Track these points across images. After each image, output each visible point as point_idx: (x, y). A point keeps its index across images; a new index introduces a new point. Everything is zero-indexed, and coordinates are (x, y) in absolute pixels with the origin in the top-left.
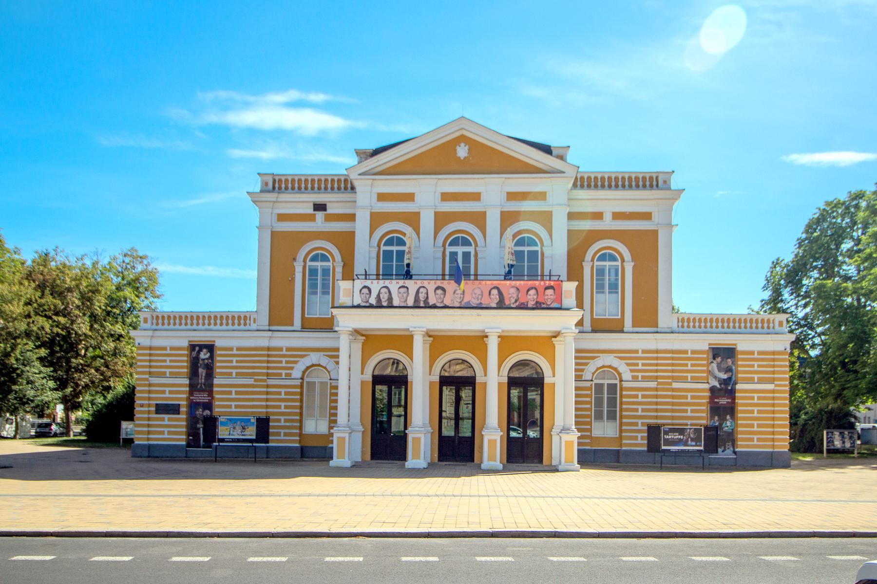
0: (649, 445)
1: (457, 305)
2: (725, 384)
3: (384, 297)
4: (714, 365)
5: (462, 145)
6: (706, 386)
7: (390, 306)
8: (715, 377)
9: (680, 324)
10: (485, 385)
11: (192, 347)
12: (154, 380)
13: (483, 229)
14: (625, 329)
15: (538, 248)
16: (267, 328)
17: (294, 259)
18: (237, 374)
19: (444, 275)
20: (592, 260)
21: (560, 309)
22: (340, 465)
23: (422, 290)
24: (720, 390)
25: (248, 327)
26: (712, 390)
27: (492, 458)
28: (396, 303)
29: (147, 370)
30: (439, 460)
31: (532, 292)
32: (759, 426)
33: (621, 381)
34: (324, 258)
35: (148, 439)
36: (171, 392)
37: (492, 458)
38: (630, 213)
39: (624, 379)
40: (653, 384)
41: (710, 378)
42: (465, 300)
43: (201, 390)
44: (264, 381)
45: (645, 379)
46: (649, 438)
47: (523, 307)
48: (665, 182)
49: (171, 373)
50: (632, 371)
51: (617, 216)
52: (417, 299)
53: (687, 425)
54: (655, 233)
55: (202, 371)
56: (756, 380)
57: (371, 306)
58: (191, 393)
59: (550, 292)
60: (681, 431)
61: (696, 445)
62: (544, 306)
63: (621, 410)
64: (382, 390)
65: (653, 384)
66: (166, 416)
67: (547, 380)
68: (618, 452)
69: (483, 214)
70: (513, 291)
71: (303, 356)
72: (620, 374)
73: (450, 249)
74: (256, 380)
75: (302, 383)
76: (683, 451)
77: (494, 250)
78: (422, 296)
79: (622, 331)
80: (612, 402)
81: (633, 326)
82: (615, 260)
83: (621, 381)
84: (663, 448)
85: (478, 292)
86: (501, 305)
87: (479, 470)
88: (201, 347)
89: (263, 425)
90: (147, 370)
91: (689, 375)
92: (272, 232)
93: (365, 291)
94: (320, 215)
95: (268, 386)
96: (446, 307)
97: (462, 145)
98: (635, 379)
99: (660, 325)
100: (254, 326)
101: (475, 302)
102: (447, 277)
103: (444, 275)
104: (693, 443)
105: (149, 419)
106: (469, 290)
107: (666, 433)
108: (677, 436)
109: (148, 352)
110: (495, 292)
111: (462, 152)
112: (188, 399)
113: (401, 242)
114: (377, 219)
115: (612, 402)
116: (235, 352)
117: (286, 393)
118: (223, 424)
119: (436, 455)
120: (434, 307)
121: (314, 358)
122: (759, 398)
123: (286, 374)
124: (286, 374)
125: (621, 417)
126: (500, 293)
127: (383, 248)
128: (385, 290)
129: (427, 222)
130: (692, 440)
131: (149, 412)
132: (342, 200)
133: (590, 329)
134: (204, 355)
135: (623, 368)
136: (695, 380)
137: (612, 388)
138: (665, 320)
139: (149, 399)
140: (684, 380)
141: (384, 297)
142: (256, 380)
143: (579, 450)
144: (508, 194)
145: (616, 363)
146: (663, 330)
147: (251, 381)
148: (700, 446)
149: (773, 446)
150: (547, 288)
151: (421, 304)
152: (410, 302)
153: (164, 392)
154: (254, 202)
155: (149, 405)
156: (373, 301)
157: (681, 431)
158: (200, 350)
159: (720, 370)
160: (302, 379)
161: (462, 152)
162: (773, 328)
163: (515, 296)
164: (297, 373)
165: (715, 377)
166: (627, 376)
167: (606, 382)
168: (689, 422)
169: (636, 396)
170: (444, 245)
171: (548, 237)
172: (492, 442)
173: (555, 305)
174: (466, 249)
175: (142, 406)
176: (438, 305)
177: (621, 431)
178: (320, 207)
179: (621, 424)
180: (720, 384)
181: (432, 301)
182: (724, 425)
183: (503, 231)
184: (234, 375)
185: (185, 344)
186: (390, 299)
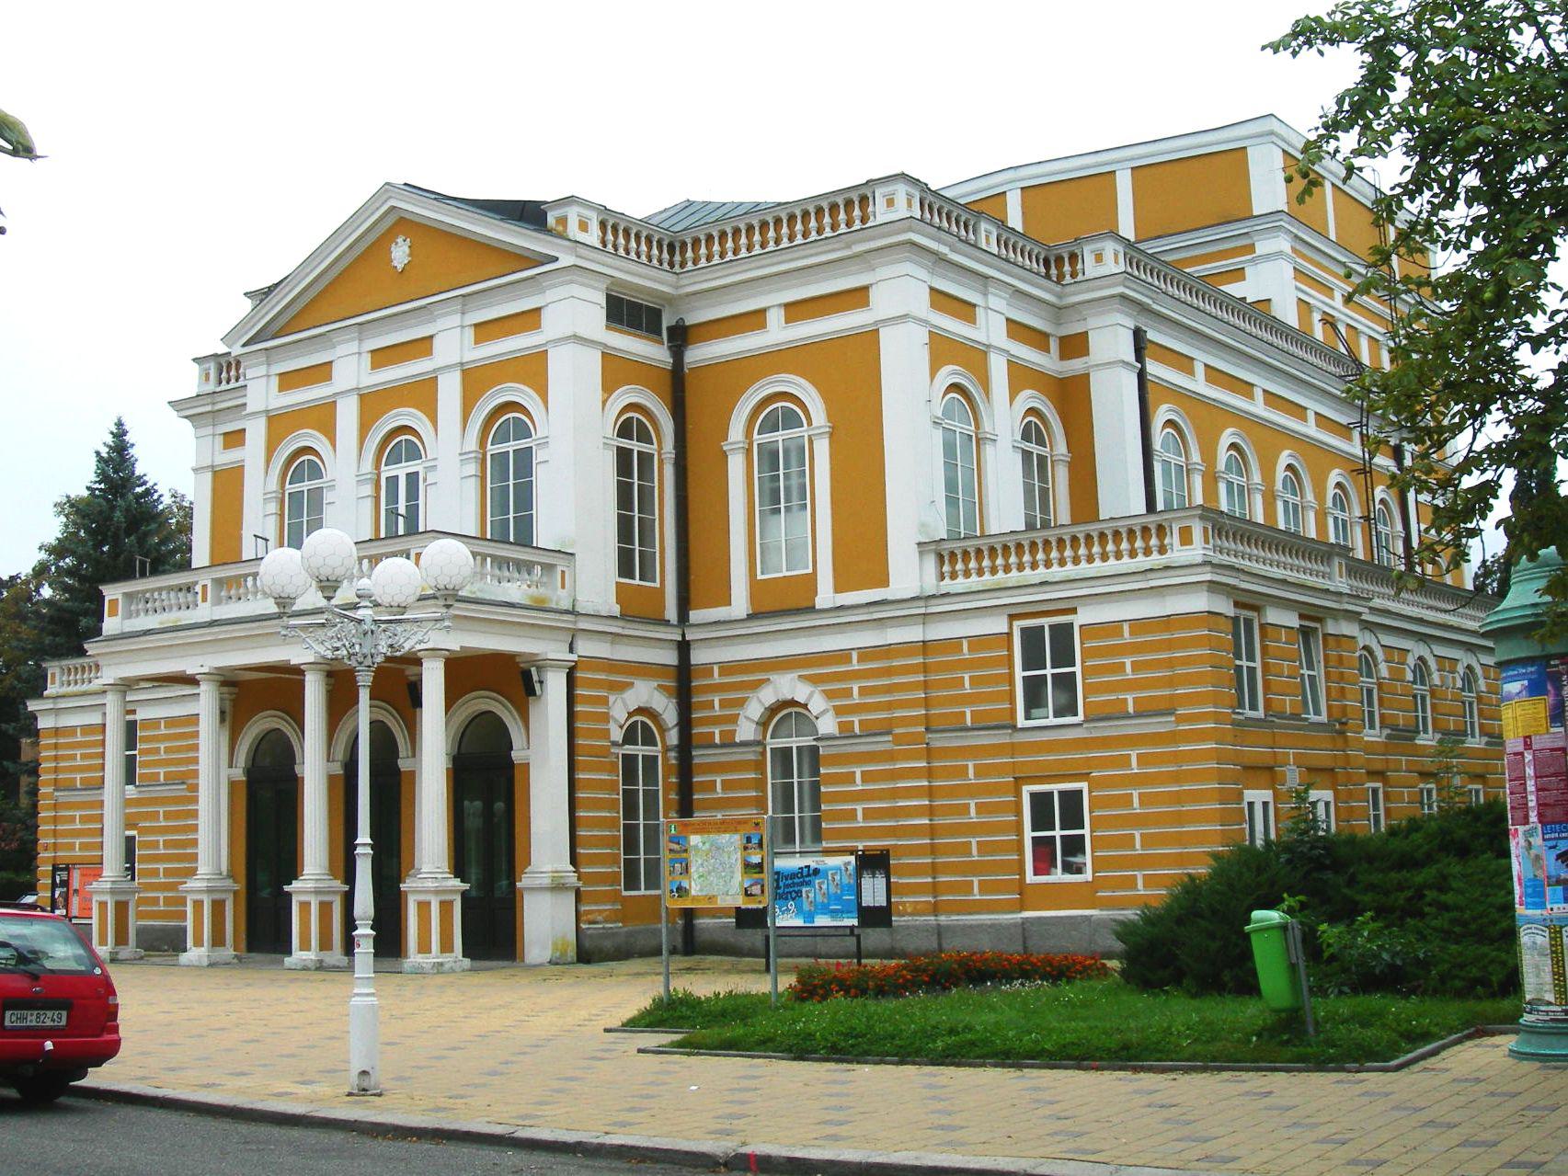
5: (400, 240)
34: (791, 420)
45: (871, 731)
50: (839, 711)
51: (796, 311)
65: (883, 743)
73: (387, 472)
79: (811, 609)
121: (787, 686)
129: (450, 391)
142: (898, 740)
145: (801, 692)
160: (761, 743)
166: (827, 725)
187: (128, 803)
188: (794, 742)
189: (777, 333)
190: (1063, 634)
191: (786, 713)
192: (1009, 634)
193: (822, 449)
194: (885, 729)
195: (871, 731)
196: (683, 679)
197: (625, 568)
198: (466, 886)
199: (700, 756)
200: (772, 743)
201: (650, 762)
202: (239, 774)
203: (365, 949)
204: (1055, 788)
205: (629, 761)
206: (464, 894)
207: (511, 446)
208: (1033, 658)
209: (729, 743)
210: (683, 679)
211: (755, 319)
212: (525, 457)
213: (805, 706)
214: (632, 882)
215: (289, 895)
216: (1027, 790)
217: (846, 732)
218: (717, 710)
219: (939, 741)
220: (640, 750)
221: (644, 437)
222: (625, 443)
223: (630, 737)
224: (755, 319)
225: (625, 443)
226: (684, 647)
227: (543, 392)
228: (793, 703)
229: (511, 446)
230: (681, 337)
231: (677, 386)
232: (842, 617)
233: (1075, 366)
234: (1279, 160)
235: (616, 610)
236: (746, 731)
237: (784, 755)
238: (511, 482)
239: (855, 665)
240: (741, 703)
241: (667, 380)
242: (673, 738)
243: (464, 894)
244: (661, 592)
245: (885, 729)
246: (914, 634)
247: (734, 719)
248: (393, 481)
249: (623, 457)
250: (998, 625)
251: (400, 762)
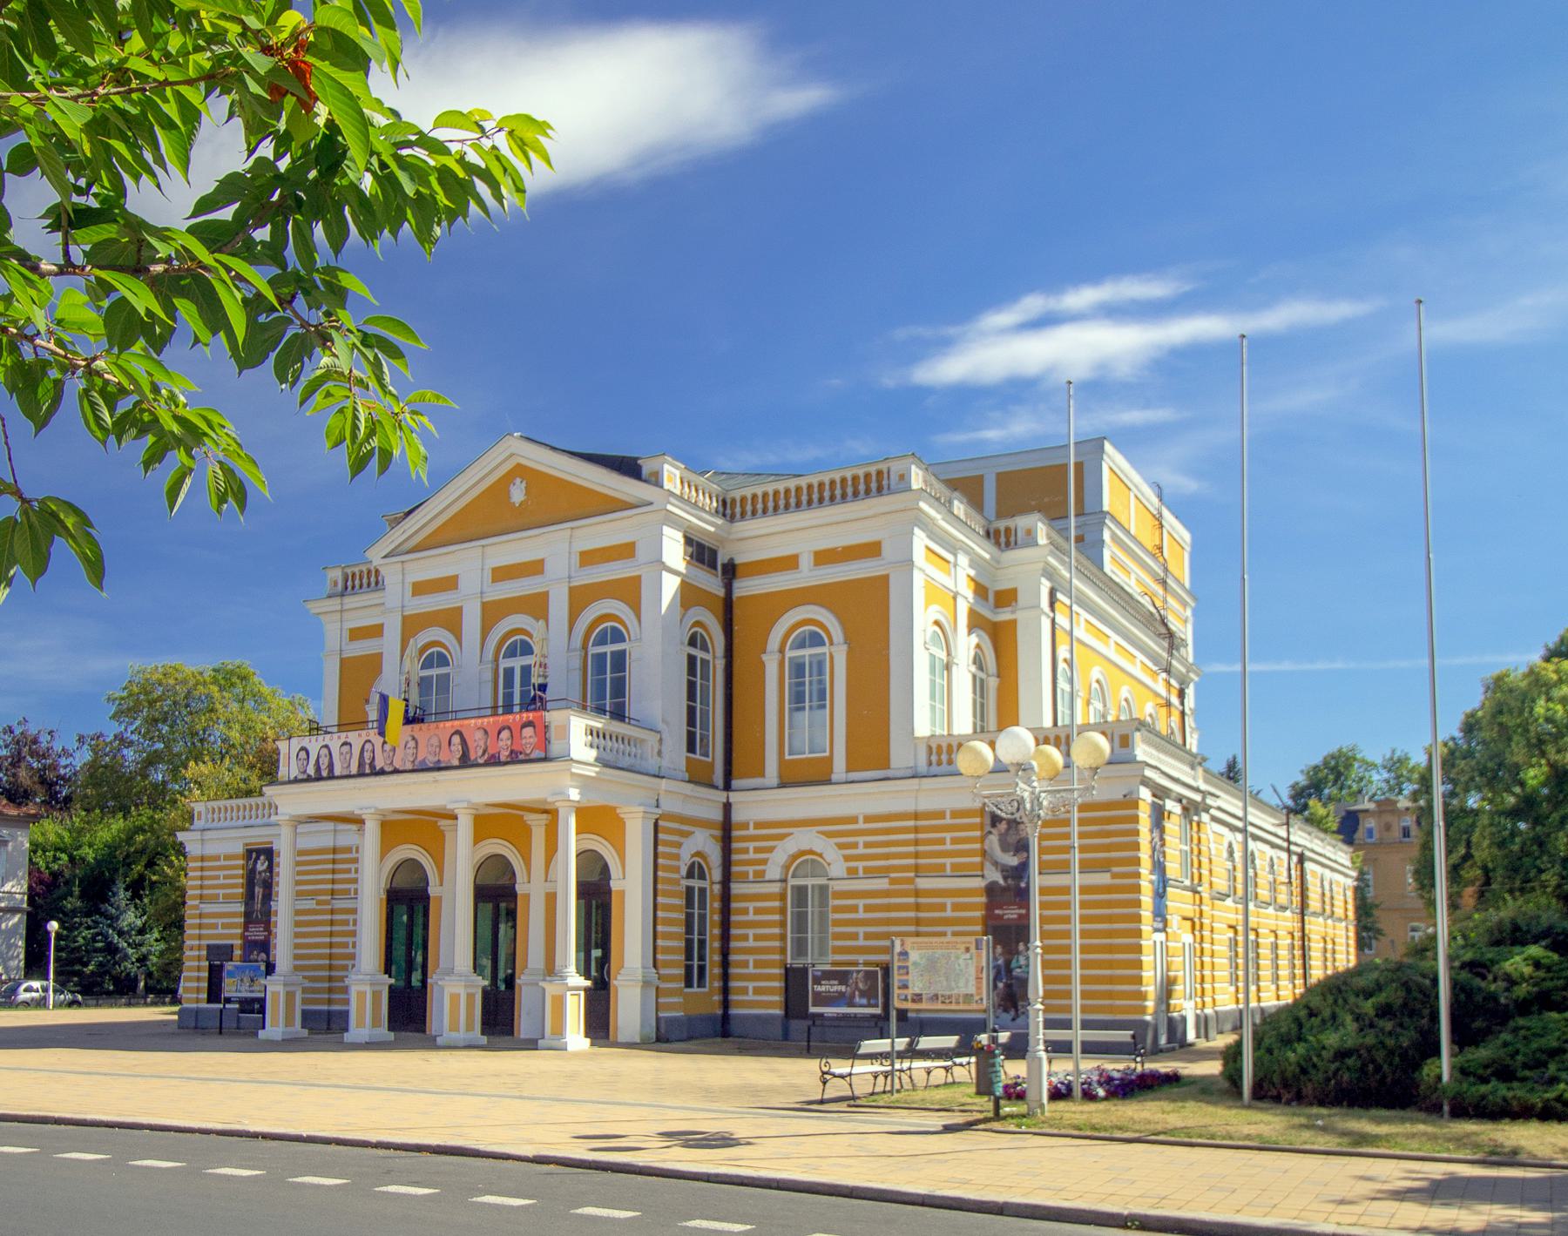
1: (409, 766)
2: (1013, 878)
3: (324, 762)
4: (994, 839)
5: (518, 480)
6: (979, 883)
7: (331, 777)
8: (996, 864)
9: (934, 758)
10: (622, 893)
11: (249, 852)
13: (457, 632)
14: (834, 777)
17: (367, 701)
18: (954, 867)
19: (495, 707)
20: (782, 651)
21: (545, 759)
23: (368, 746)
24: (1005, 890)
26: (991, 890)
27: (454, 1027)
28: (337, 771)
29: (912, 861)
31: (505, 734)
34: (816, 640)
37: (454, 1027)
38: (846, 549)
40: (882, 884)
41: (988, 865)
42: (420, 758)
43: (257, 922)
44: (910, 881)
45: (871, 873)
47: (494, 761)
48: (902, 477)
49: (225, 896)
50: (847, 858)
51: (824, 558)
52: (361, 764)
53: (856, 964)
54: (885, 579)
55: (258, 891)
56: (751, 877)
57: (309, 779)
58: (246, 927)
59: (528, 731)
60: (842, 977)
61: (869, 1005)
62: (521, 757)
65: (882, 884)
67: (433, 890)
69: (459, 611)
70: (479, 735)
71: (781, 837)
73: (505, 664)
74: (893, 881)
76: (845, 1017)
77: (472, 667)
78: (367, 755)
79: (828, 782)
81: (848, 770)
84: (813, 1010)
85: (435, 741)
86: (466, 762)
87: (432, 1044)
88: (259, 852)
90: (912, 861)
91: (948, 861)
92: (342, 660)
93: (303, 754)
95: (332, 912)
96: (396, 771)
97: (518, 480)
98: (852, 873)
99: (894, 764)
101: (431, 760)
102: (500, 711)
103: (495, 707)
104: (864, 1001)
106: (431, 737)
107: (817, 981)
108: (834, 987)
109: (911, 823)
110: (456, 739)
111: (518, 494)
112: (243, 937)
113: (618, 636)
114: (412, 625)
116: (861, 825)
117: (868, 908)
118: (231, 974)
120: (382, 772)
122: (956, 907)
123: (756, 873)
124: (756, 873)
126: (464, 742)
127: (593, 650)
128: (325, 751)
129: (559, 607)
130: (862, 994)
132: (814, 523)
133: (775, 781)
134: (261, 866)
136: (960, 872)
140: (939, 871)
141: (324, 762)
142: (893, 881)
144: (583, 554)
146: (899, 774)
148: (876, 1006)
150: (525, 726)
151: (366, 770)
152: (354, 770)
156: (311, 771)
157: (842, 977)
158: (258, 858)
159: (1005, 847)
160: (784, 881)
161: (518, 494)
163: (482, 743)
165: (996, 864)
166: (838, 868)
168: (861, 959)
169: (942, 907)
171: (636, 622)
172: (455, 998)
173: (537, 754)
176: (388, 769)
180: (1005, 878)
181: (379, 765)
182: (1014, 964)
183: (485, 631)
184: (861, 874)
185: (240, 850)
186: (331, 766)
187: (298, 912)
188: (809, 882)
189: (807, 576)
191: (807, 861)
196: (726, 831)
197: (691, 747)
198: (392, 981)
199: (736, 888)
200: (792, 882)
201: (702, 891)
205: (690, 890)
206: (391, 987)
207: (609, 649)
210: (726, 831)
212: (620, 660)
213: (821, 855)
214: (689, 984)
218: (751, 855)
219: (924, 883)
220: (696, 883)
221: (705, 648)
222: (694, 652)
223: (690, 875)
225: (694, 652)
226: (727, 807)
227: (636, 608)
228: (811, 852)
229: (609, 649)
230: (730, 572)
231: (727, 610)
233: (1004, 616)
234: (679, 536)
235: (687, 776)
236: (773, 872)
237: (801, 892)
238: (608, 676)
240: (771, 850)
241: (720, 607)
242: (717, 875)
243: (391, 987)
244: (712, 765)
247: (764, 862)
248: (509, 673)
249: (692, 660)
251: (612, 883)
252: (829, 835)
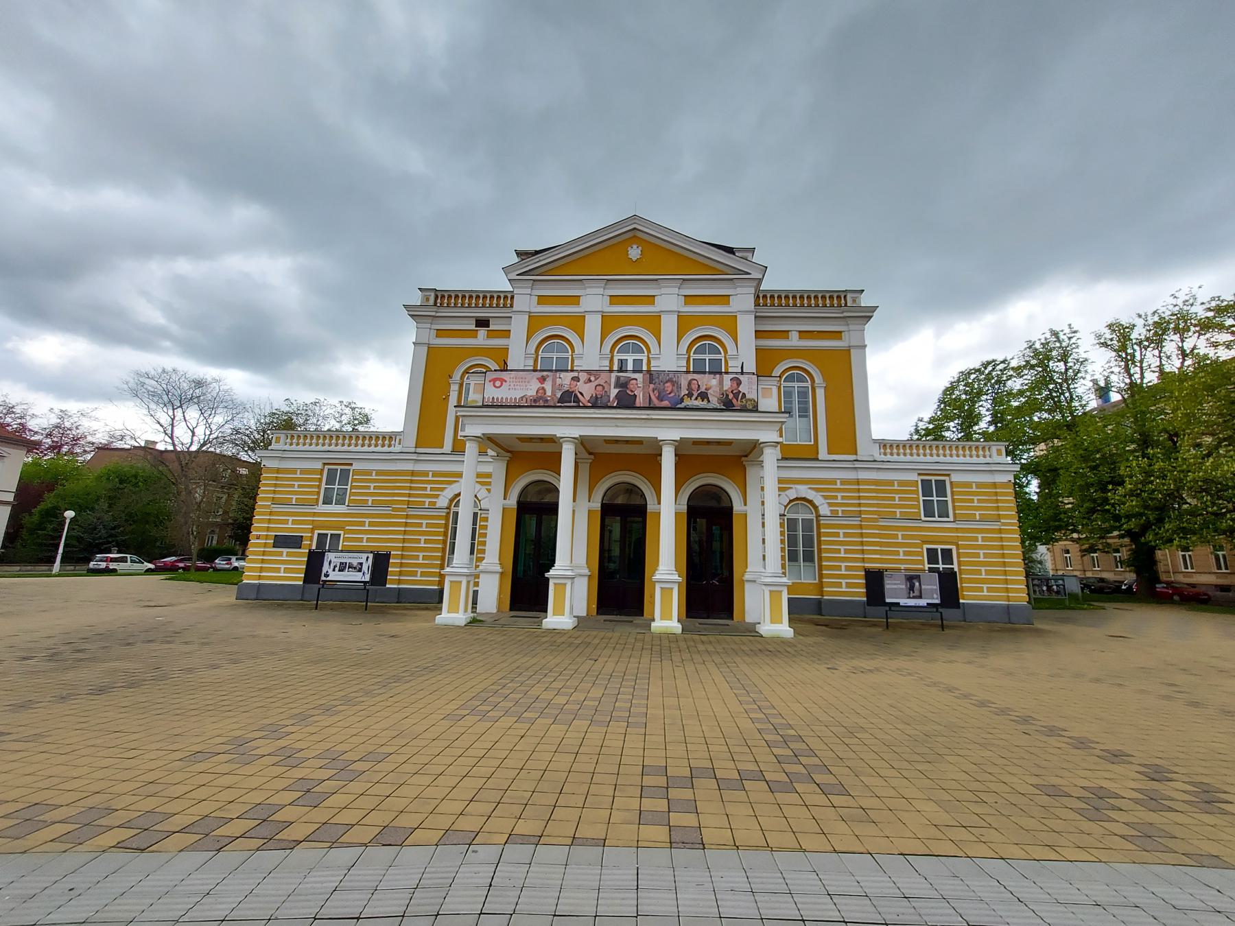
0: (868, 594)
10: (658, 515)
12: (276, 508)
15: (722, 356)
16: (413, 450)
17: (450, 377)
22: (450, 622)
25: (392, 449)
30: (598, 613)
32: (846, 551)
33: (818, 516)
35: (260, 577)
36: (294, 522)
39: (822, 513)
44: (876, 520)
45: (846, 515)
46: (868, 586)
50: (830, 505)
63: (820, 550)
64: (532, 522)
66: (285, 551)
68: (819, 602)
72: (816, 507)
75: (448, 513)
80: (808, 541)
82: (804, 380)
83: (818, 516)
89: (381, 562)
94: (482, 332)
100: (398, 448)
105: (264, 553)
115: (808, 541)
119: (595, 606)
125: (820, 559)
131: (265, 545)
135: (818, 499)
137: (807, 524)
138: (865, 450)
139: (268, 529)
143: (791, 601)
145: (811, 495)
147: (388, 511)
149: (1008, 599)
153: (286, 522)
154: (412, 316)
155: (267, 537)
162: (468, 582)
164: (443, 502)
166: (824, 510)
167: (800, 517)
170: (612, 351)
172: (666, 616)
174: (638, 356)
175: (258, 537)
177: (821, 576)
178: (482, 323)
179: (820, 567)
189: (794, 341)
190: (941, 485)
192: (322, 470)
193: (820, 393)
194: (387, 504)
195: (846, 515)
202: (684, 508)
203: (666, 613)
204: (939, 547)
208: (927, 491)
209: (433, 506)
211: (785, 334)
215: (548, 579)
216: (317, 532)
217: (834, 514)
224: (785, 334)
232: (831, 465)
239: (839, 486)
240: (442, 489)
245: (387, 504)
246: (409, 467)
247: (437, 496)
250: (914, 477)
252: (817, 490)
